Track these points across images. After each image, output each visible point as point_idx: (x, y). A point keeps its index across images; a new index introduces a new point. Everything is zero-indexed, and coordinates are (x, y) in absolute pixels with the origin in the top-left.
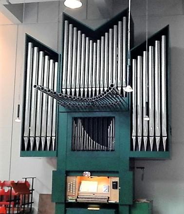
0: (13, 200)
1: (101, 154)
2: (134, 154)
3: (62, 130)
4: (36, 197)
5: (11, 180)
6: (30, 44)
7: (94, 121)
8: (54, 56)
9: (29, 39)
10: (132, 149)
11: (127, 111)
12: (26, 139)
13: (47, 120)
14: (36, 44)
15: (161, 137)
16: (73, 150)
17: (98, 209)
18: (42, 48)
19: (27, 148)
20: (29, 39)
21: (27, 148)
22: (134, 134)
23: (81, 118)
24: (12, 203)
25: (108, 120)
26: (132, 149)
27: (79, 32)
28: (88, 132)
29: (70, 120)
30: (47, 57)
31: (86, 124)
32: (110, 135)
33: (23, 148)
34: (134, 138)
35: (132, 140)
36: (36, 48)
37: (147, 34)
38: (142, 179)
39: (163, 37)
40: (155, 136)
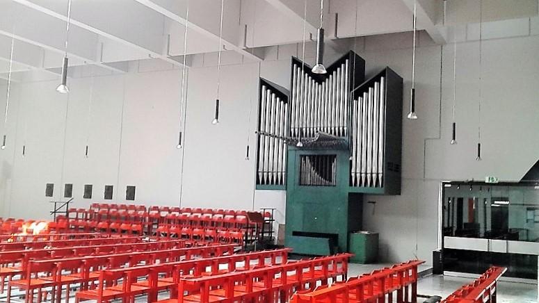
0: (250, 228)
1: (325, 189)
2: (357, 190)
3: (291, 167)
4: (275, 227)
5: (255, 211)
6: (264, 87)
7: (323, 155)
8: (283, 97)
9: (263, 82)
10: (351, 185)
11: (348, 149)
12: (260, 174)
13: (277, 159)
14: (269, 86)
15: (378, 174)
16: (300, 185)
17: (506, 269)
18: (274, 90)
19: (262, 182)
20: (263, 82)
21: (262, 182)
22: (353, 171)
23: (310, 156)
24: (249, 230)
25: (332, 158)
26: (351, 185)
27: (310, 78)
28: (317, 171)
29: (298, 158)
30: (278, 99)
31: (314, 161)
32: (333, 171)
33: (258, 182)
34: (353, 175)
35: (351, 177)
36: (273, 95)
37: (531, 181)
38: (373, 214)
39: (382, 78)
40: (372, 174)
